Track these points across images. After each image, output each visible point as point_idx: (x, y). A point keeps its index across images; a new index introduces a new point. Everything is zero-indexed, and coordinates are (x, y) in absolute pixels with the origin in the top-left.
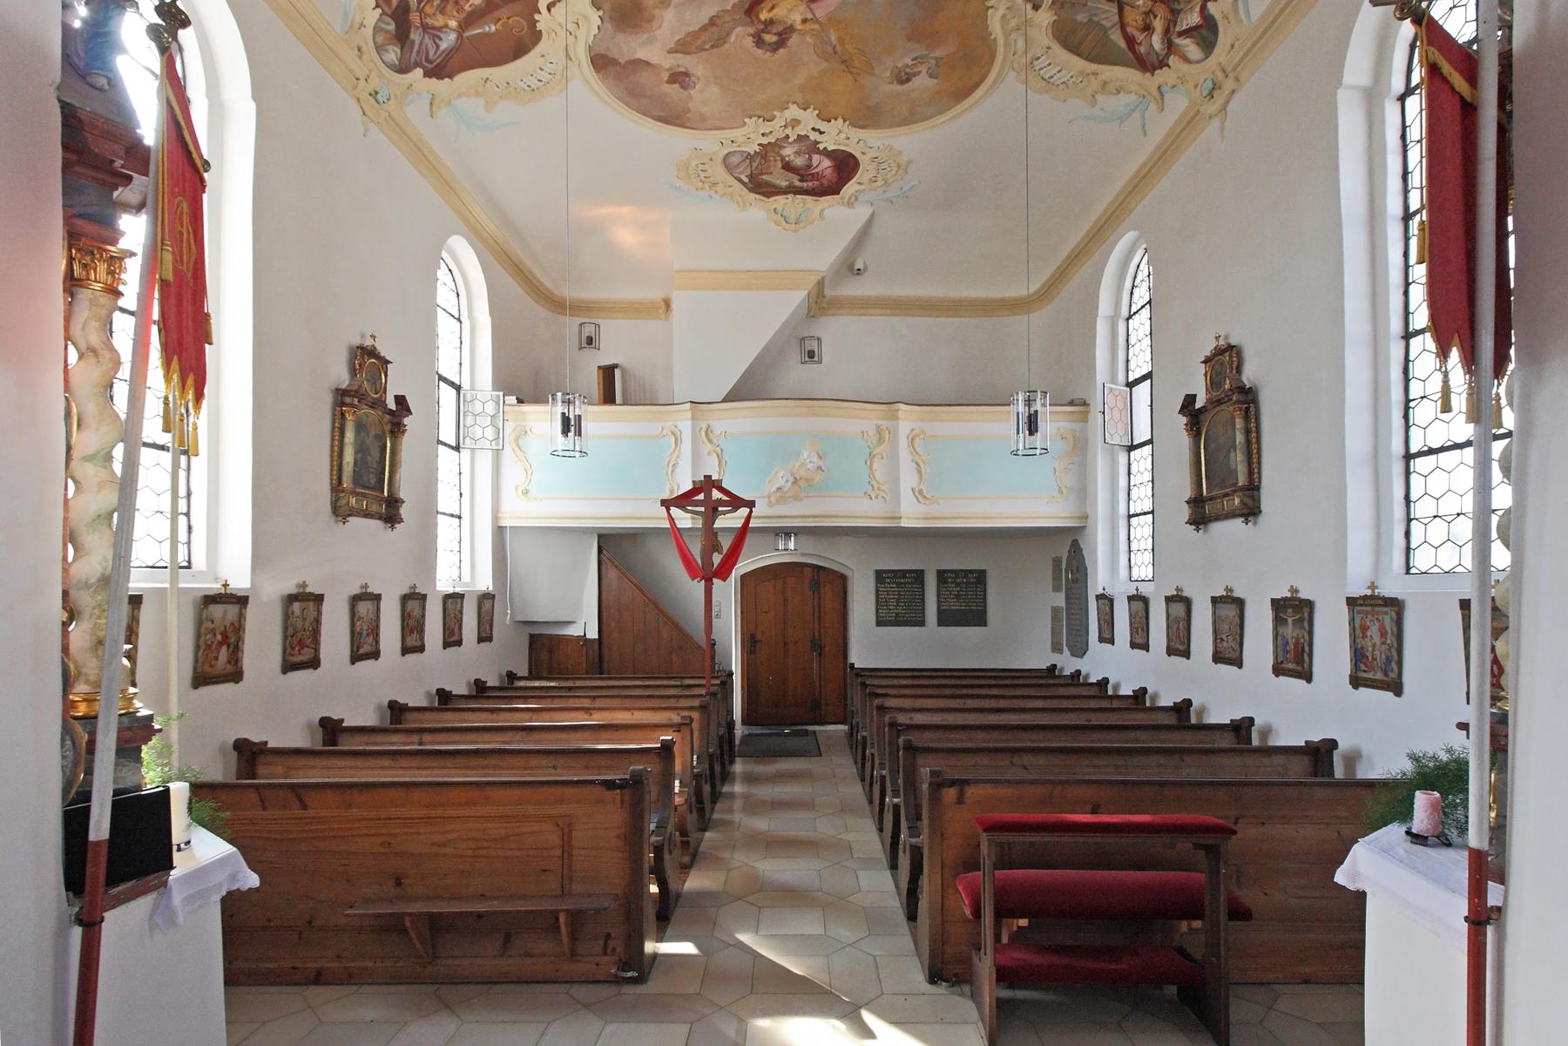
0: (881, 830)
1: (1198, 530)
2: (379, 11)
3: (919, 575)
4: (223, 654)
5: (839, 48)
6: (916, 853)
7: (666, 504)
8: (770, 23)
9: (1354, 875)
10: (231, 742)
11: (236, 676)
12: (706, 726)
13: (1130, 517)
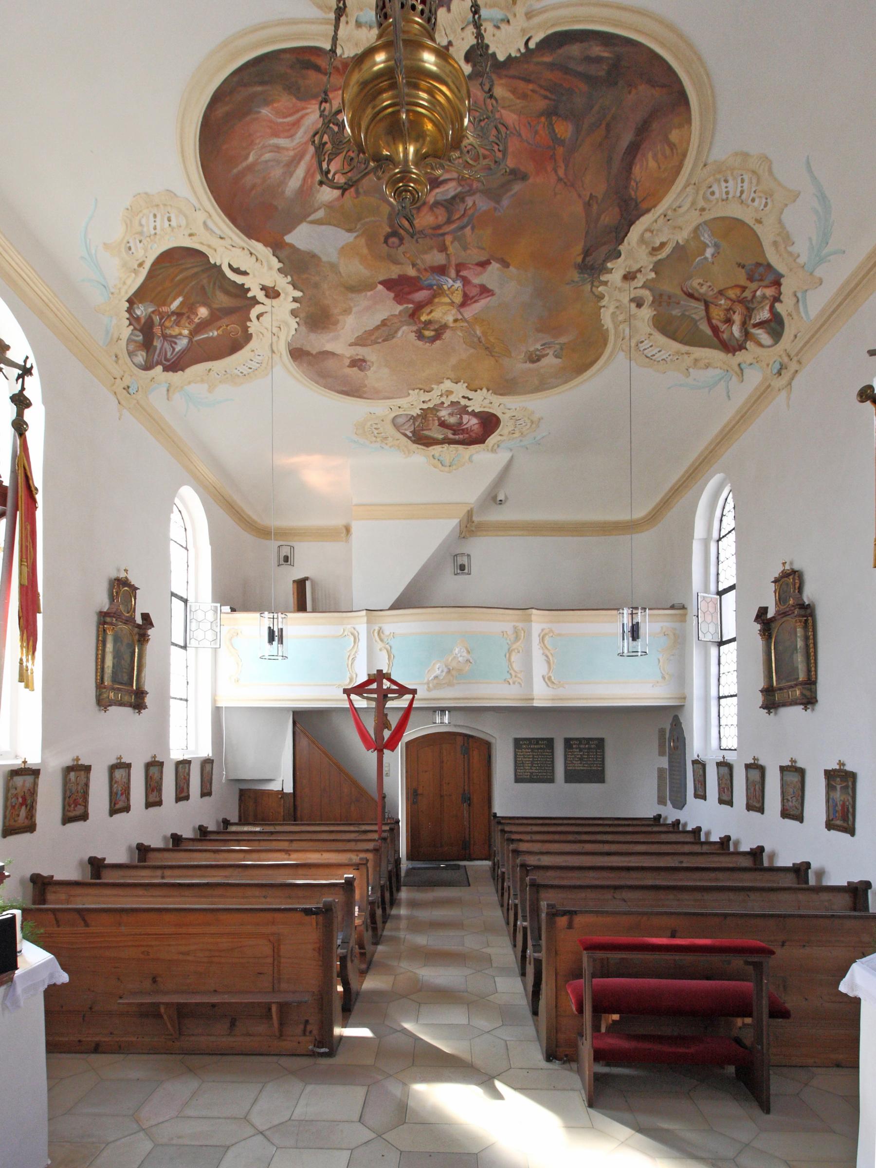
0: (515, 946)
1: (769, 713)
2: (131, 327)
3: (550, 742)
4: (23, 812)
5: (483, 339)
6: (538, 963)
7: (348, 692)
8: (428, 323)
9: (853, 986)
10: (29, 876)
11: (31, 828)
12: (378, 865)
13: (720, 698)
